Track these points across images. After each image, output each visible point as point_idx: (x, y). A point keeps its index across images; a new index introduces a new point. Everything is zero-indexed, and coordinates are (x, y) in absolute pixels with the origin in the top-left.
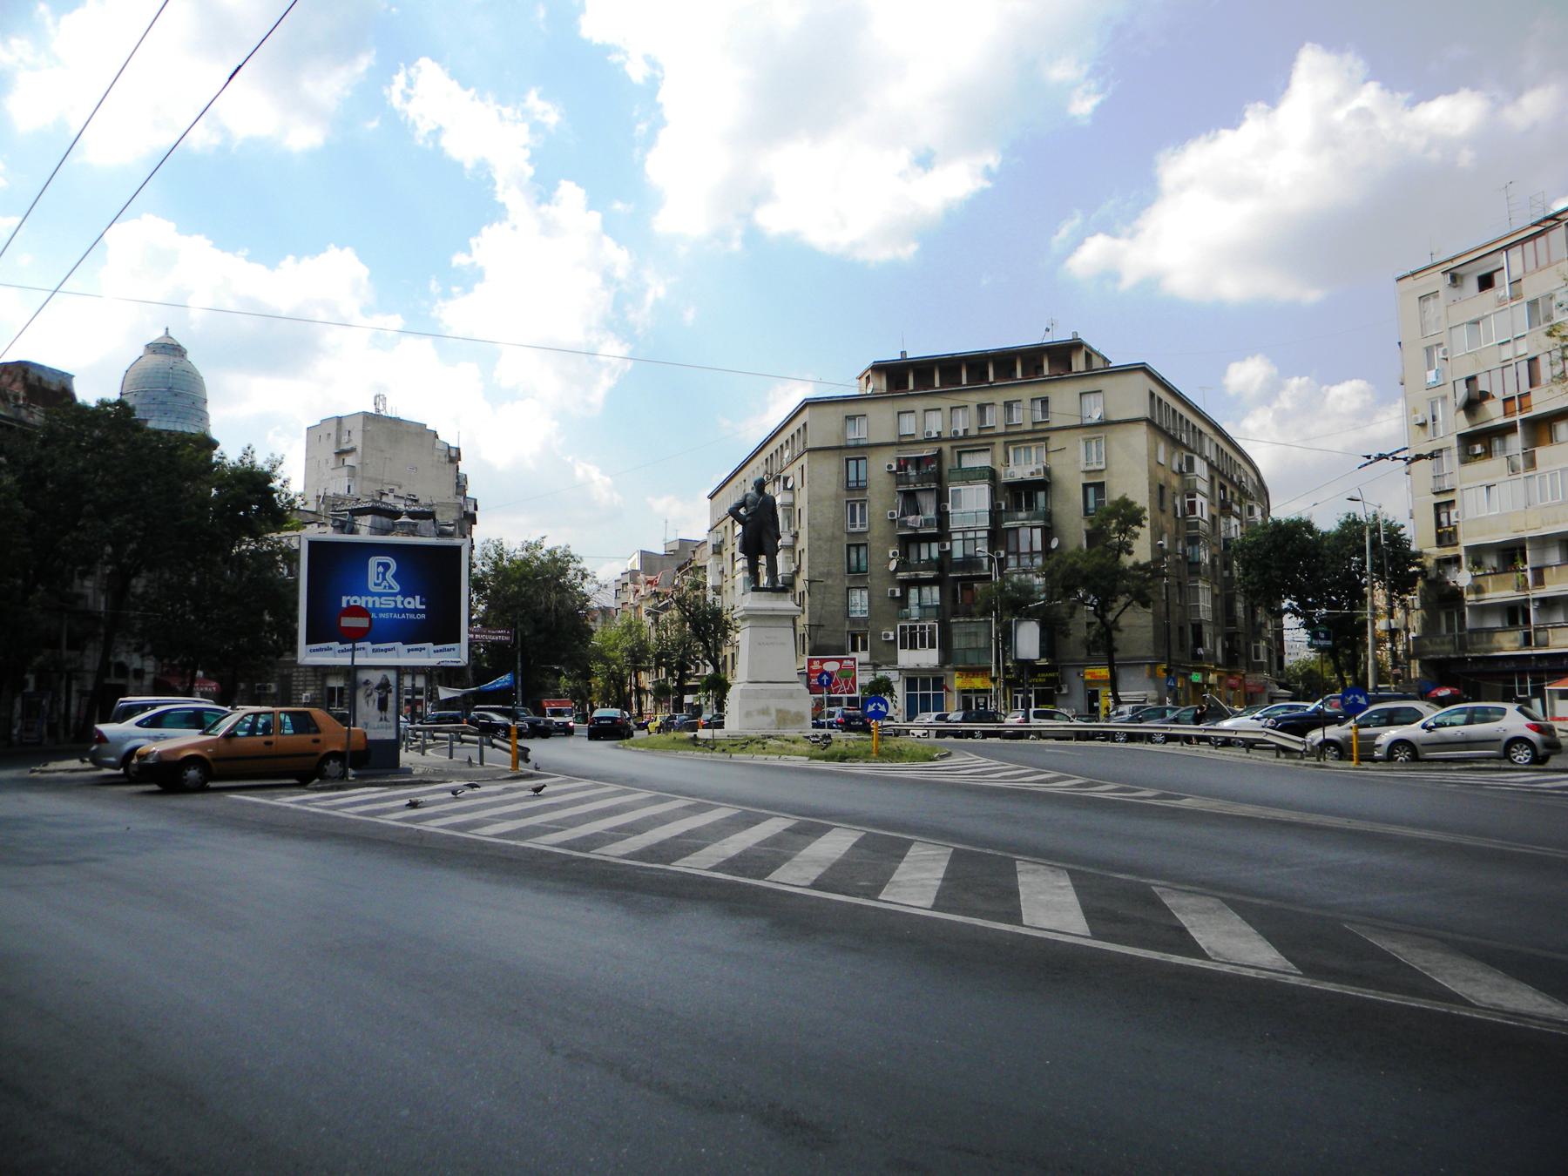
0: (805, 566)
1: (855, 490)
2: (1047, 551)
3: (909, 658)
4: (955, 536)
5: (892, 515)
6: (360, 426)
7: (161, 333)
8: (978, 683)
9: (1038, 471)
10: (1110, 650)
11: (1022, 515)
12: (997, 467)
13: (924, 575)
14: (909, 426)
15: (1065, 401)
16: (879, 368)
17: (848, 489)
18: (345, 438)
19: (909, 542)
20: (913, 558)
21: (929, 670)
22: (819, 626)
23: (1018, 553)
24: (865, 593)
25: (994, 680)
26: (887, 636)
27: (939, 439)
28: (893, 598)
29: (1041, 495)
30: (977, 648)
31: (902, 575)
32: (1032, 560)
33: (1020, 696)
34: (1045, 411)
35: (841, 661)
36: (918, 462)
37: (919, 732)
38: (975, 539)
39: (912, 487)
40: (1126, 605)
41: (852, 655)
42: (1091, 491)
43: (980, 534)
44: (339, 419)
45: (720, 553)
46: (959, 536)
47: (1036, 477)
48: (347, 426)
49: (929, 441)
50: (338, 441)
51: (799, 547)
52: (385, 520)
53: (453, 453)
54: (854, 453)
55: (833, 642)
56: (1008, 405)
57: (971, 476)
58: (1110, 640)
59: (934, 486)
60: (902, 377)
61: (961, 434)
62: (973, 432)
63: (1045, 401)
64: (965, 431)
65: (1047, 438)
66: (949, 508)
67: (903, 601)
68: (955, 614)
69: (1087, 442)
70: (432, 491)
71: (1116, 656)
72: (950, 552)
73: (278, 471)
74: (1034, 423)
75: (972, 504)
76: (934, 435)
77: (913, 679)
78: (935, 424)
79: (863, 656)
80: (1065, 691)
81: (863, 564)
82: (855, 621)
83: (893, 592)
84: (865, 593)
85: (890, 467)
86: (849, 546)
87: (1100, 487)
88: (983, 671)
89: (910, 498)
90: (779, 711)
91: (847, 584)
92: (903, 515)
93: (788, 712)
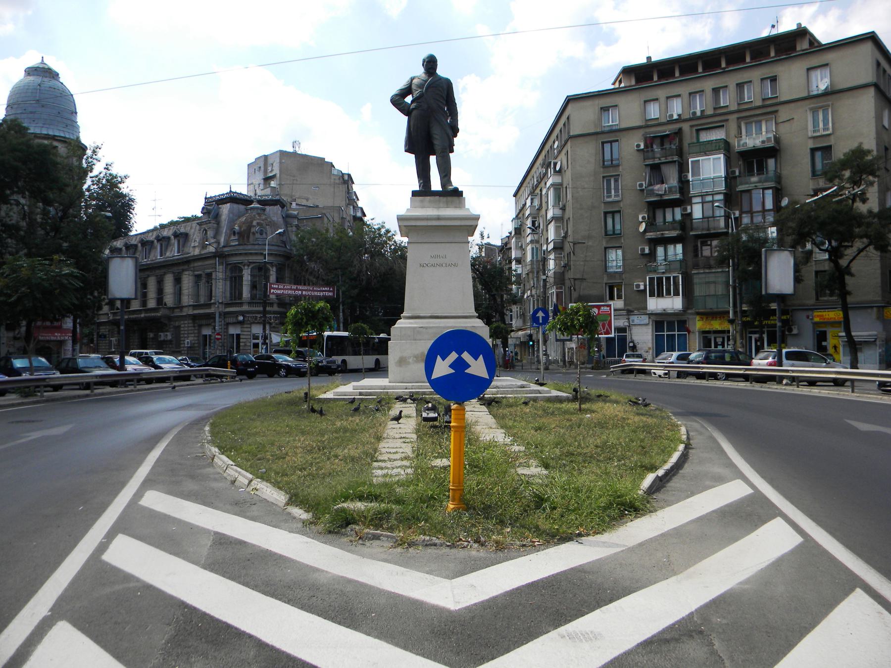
0: (570, 233)
1: (609, 170)
2: (777, 208)
3: (655, 304)
4: (695, 200)
5: (641, 185)
6: (278, 160)
7: (40, 61)
8: (716, 325)
9: (769, 139)
10: (844, 294)
11: (754, 179)
14: (654, 111)
15: (792, 78)
16: (628, 71)
17: (604, 166)
18: (270, 169)
19: (657, 206)
20: (659, 220)
21: (675, 314)
22: (582, 279)
23: (751, 212)
24: (620, 252)
25: (732, 322)
26: (638, 286)
27: (680, 120)
28: (643, 255)
29: (771, 162)
31: (650, 235)
32: (764, 218)
33: (754, 336)
35: (598, 307)
36: (663, 139)
37: (661, 373)
38: (713, 202)
39: (657, 161)
40: (860, 251)
41: (611, 303)
42: (818, 155)
45: (520, 234)
46: (699, 200)
47: (767, 145)
48: (270, 161)
49: (671, 122)
50: (265, 171)
51: (566, 217)
52: (242, 207)
53: (346, 178)
56: (740, 86)
57: (708, 149)
58: (843, 284)
59: (676, 158)
60: (644, 76)
61: (698, 114)
62: (710, 112)
63: (774, 79)
64: (702, 112)
65: (777, 111)
67: (652, 255)
68: (696, 266)
69: (814, 111)
70: (325, 199)
71: (849, 299)
72: (690, 214)
73: (100, 154)
74: (764, 100)
75: (712, 168)
76: (675, 117)
77: (661, 321)
78: (676, 108)
79: (618, 304)
80: (795, 331)
81: (618, 227)
82: (613, 275)
83: (643, 250)
84: (620, 252)
85: (638, 146)
86: (606, 213)
87: (827, 150)
88: (721, 314)
89: (655, 169)
91: (605, 245)
92: (650, 184)
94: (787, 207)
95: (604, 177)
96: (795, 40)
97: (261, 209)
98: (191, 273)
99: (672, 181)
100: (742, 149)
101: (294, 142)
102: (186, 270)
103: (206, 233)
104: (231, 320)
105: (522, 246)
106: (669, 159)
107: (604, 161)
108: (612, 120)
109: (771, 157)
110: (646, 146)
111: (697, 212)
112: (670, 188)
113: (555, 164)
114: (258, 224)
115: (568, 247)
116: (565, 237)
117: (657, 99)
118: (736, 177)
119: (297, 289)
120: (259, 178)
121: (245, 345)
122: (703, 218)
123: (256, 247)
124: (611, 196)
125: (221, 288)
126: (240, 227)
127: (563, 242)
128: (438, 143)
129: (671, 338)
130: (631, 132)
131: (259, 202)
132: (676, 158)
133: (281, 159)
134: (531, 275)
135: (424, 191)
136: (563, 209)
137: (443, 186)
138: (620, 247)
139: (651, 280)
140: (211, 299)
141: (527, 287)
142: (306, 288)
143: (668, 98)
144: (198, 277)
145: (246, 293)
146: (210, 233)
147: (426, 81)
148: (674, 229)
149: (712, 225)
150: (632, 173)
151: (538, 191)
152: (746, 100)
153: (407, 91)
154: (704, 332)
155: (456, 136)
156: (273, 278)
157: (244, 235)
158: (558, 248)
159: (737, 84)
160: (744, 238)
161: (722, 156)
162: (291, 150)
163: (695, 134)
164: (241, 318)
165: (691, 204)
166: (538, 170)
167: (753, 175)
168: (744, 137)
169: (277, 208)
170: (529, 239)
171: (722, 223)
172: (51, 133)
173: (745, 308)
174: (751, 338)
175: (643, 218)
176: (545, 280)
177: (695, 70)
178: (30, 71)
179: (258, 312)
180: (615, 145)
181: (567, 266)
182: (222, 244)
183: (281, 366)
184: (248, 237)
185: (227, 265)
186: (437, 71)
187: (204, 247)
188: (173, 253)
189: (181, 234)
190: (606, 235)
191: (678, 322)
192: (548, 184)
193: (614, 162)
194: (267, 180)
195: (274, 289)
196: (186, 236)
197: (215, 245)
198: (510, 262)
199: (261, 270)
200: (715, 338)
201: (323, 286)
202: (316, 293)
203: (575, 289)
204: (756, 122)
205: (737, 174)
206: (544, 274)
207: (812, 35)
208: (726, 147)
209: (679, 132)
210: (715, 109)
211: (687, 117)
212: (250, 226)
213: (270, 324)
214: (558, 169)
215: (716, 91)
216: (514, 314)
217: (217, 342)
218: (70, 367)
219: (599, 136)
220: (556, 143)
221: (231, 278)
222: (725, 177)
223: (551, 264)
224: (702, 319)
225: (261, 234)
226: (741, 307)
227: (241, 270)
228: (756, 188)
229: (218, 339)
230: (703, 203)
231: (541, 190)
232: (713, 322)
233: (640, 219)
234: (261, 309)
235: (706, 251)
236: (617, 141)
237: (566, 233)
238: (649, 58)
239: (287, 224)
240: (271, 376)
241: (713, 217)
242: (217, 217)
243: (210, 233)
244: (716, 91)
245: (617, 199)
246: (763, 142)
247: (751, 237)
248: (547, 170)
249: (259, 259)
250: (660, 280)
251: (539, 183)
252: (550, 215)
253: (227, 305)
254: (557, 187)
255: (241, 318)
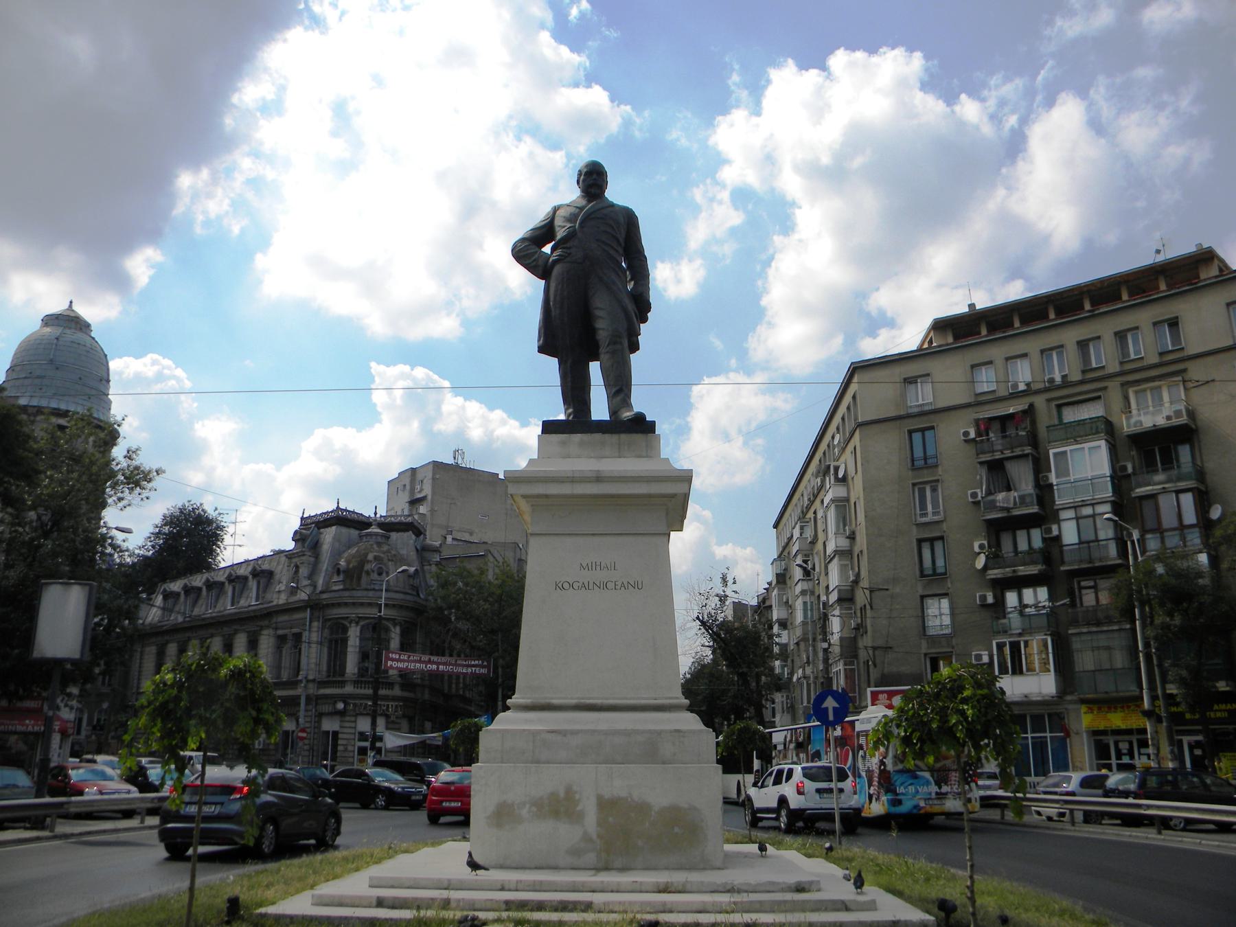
0: (864, 573)
1: (922, 469)
2: (1206, 525)
4: (1064, 515)
5: (974, 495)
6: (430, 475)
7: (66, 306)
8: (1117, 720)
9: (1178, 413)
11: (1160, 477)
12: (1114, 419)
13: (1023, 570)
14: (987, 381)
16: (940, 326)
17: (914, 468)
19: (1000, 528)
20: (1007, 546)
21: (1044, 703)
22: (887, 648)
23: (1159, 530)
24: (945, 603)
25: (1148, 714)
26: (979, 657)
27: (1028, 392)
28: (984, 606)
30: (1113, 670)
31: (994, 573)
32: (1183, 538)
34: (1176, 337)
37: (1052, 811)
38: (1093, 516)
39: (998, 456)
43: (1100, 509)
44: (413, 470)
45: (784, 583)
46: (1070, 514)
47: (1175, 421)
48: (419, 476)
49: (1015, 395)
51: (856, 550)
52: (354, 533)
54: (918, 424)
55: (905, 669)
56: (1121, 336)
59: (1028, 450)
61: (1058, 379)
62: (1076, 376)
63: (1174, 323)
64: (1064, 377)
65: (1185, 370)
66: (1053, 479)
67: (1000, 603)
68: (1075, 622)
72: (1058, 538)
75: (1087, 465)
76: (1022, 387)
78: (1023, 374)
81: (940, 563)
82: (934, 640)
83: (984, 598)
84: (945, 603)
85: (966, 434)
86: (920, 542)
89: (996, 468)
90: (606, 805)
91: (921, 591)
92: (989, 493)
93: (643, 808)
94: (1220, 520)
95: (914, 485)
96: (1197, 268)
97: (382, 536)
98: (271, 631)
99: (1023, 486)
100: (1138, 429)
101: (456, 451)
102: (268, 627)
103: (297, 572)
104: (326, 708)
105: (787, 602)
106: (1018, 452)
107: (913, 460)
108: (923, 396)
109: (1183, 442)
110: (979, 434)
111: (1069, 533)
112: (1022, 498)
113: (837, 469)
114: (376, 558)
115: (861, 598)
116: (856, 582)
117: (990, 362)
118: (1129, 476)
119: (430, 662)
120: (405, 497)
121: (346, 750)
122: (1081, 543)
123: (371, 594)
124: (925, 515)
125: (313, 658)
126: (348, 562)
127: (852, 590)
128: (603, 327)
129: (1040, 745)
130: (953, 413)
131: (381, 525)
132: (1028, 450)
133: (434, 474)
134: (802, 645)
135: (576, 422)
136: (852, 537)
137: (614, 412)
138: (945, 595)
139: (1000, 647)
140: (298, 675)
141: (798, 663)
142: (444, 659)
143: (1007, 359)
144: (281, 639)
145: (351, 665)
146: (304, 571)
147: (581, 209)
148: (1033, 563)
149: (1095, 554)
150: (959, 477)
151: (810, 515)
152: (1133, 356)
153: (544, 233)
154: (1095, 733)
155: (645, 320)
156: (395, 643)
157: (353, 575)
158: (846, 599)
159: (1116, 334)
160: (1160, 569)
161: (1103, 443)
162: (450, 461)
163: (1054, 412)
164: (340, 706)
165: (1058, 521)
166: (811, 481)
167: (1156, 471)
168: (1134, 412)
169: (409, 536)
170: (798, 589)
171: (1113, 550)
172: (63, 407)
173: (1172, 689)
174: (1181, 741)
175: (981, 546)
176: (825, 650)
177: (1045, 317)
178: (50, 320)
179: (367, 697)
180: (928, 434)
181: (860, 629)
182: (319, 588)
183: (379, 790)
184: (359, 578)
185: (325, 621)
186: (607, 194)
187: (293, 591)
188: (249, 601)
189: (263, 571)
190: (922, 575)
191: (1050, 715)
192: (826, 501)
193: (929, 461)
194: (414, 502)
195: (393, 660)
196: (270, 574)
197: (308, 590)
198: (771, 627)
199: (376, 630)
200: (1116, 744)
201: (467, 657)
202: (460, 670)
203: (875, 666)
204: (1152, 389)
205: (1130, 470)
206: (825, 640)
207: (1222, 261)
208: (1108, 428)
209: (1030, 411)
210: (1084, 372)
211: (1041, 386)
212: (363, 562)
213: (387, 716)
214: (840, 475)
215: (1083, 345)
216: (778, 707)
217: (300, 744)
218: (63, 786)
219: (906, 421)
220: (837, 437)
221: (330, 641)
222: (1111, 477)
223: (835, 625)
224: (1091, 710)
225: (380, 574)
226: (1164, 689)
227: (345, 630)
228: (1165, 491)
229: (302, 739)
230: (1077, 518)
231: (815, 513)
232: (1110, 716)
233: (977, 549)
234: (370, 692)
235: (1089, 599)
236: (932, 428)
237: (858, 575)
238: (972, 306)
239: (423, 561)
240: (365, 806)
241: (1097, 540)
242: (316, 546)
243: (304, 571)
244: (1083, 345)
245: (936, 518)
246: (1169, 418)
247: (1170, 569)
248: (823, 481)
249: (373, 612)
250: (1015, 647)
251: (812, 502)
252: (831, 548)
253: (322, 684)
254: (842, 504)
255: (340, 706)
